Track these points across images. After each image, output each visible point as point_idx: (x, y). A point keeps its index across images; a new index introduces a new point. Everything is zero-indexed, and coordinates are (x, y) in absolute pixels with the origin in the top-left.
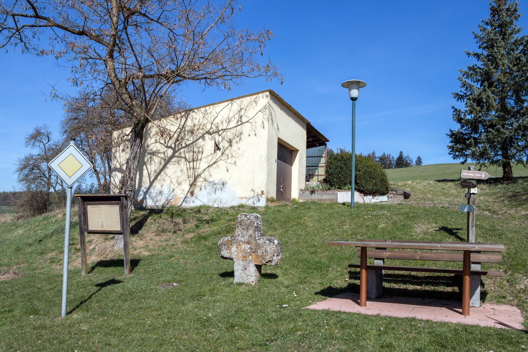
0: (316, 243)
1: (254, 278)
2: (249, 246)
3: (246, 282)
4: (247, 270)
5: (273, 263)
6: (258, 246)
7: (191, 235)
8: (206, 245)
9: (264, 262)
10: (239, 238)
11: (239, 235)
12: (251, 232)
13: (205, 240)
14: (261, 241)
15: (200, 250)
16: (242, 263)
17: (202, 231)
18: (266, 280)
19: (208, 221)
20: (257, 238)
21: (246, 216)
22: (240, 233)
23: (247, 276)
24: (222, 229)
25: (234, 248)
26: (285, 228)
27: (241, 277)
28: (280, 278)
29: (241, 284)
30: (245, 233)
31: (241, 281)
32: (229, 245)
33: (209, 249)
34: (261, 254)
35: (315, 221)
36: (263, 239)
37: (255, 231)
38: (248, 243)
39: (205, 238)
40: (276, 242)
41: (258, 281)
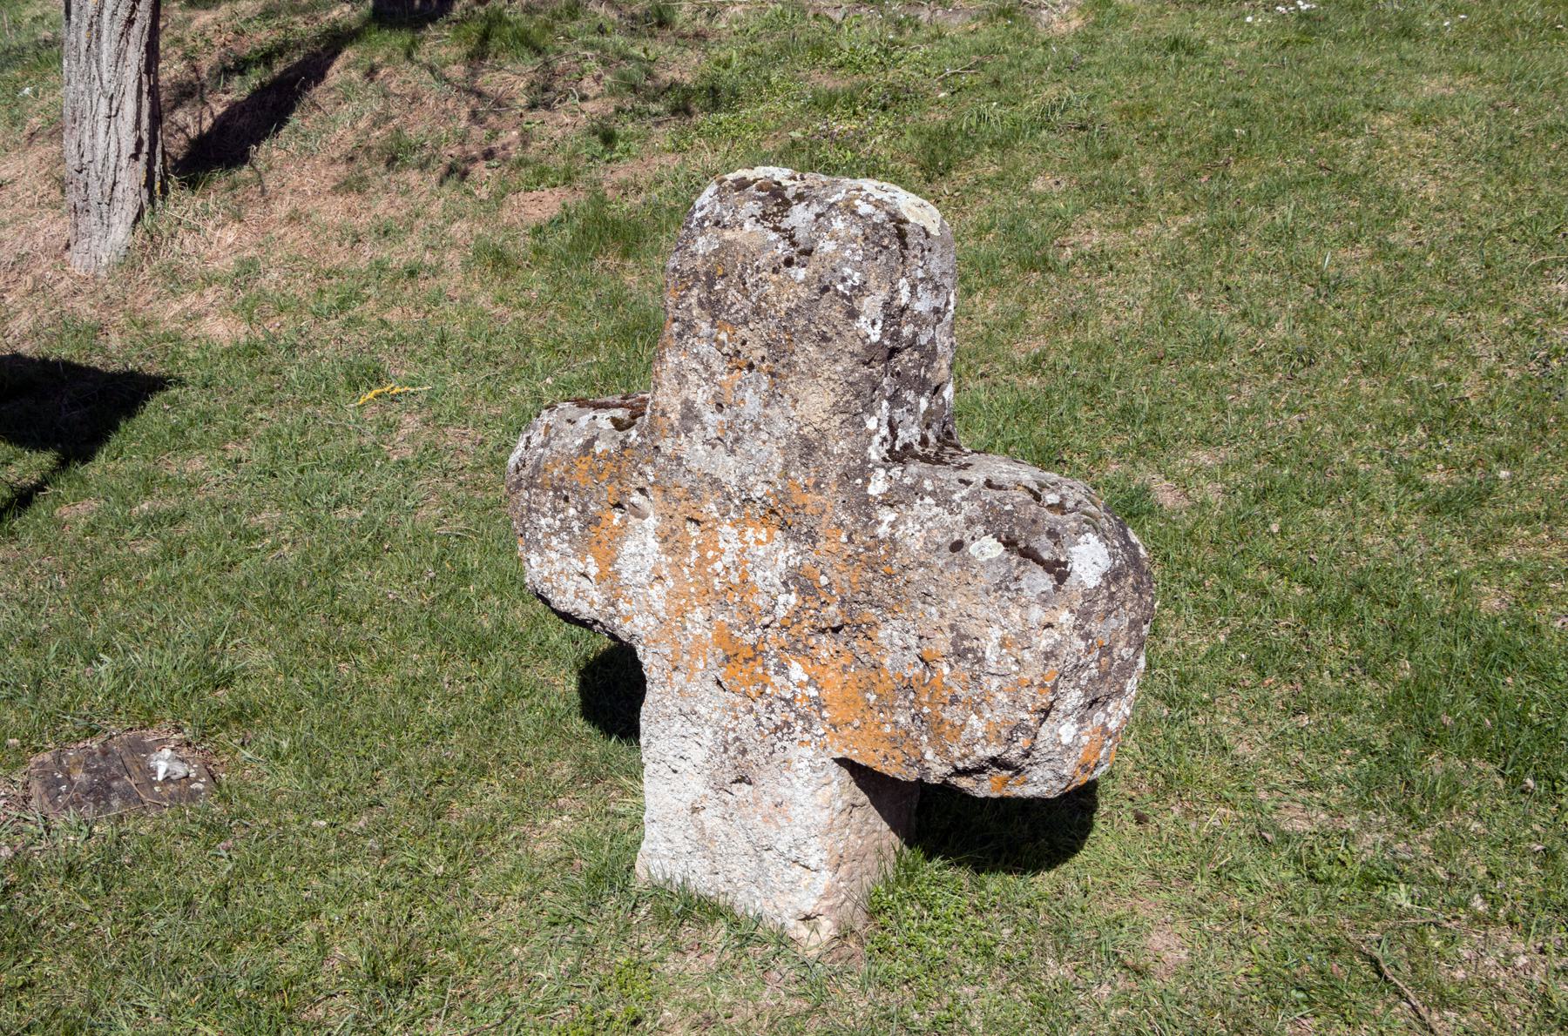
0: (1470, 387)
1: (825, 879)
3: (748, 901)
6: (882, 575)
7: (545, 204)
10: (696, 453)
12: (815, 403)
14: (914, 529)
16: (711, 703)
18: (950, 885)
19: (688, 94)
20: (877, 487)
22: (701, 397)
23: (760, 849)
25: (641, 548)
27: (704, 842)
30: (752, 403)
31: (702, 881)
32: (593, 498)
35: (1464, 155)
36: (943, 499)
37: (860, 398)
38: (781, 515)
40: (1090, 559)
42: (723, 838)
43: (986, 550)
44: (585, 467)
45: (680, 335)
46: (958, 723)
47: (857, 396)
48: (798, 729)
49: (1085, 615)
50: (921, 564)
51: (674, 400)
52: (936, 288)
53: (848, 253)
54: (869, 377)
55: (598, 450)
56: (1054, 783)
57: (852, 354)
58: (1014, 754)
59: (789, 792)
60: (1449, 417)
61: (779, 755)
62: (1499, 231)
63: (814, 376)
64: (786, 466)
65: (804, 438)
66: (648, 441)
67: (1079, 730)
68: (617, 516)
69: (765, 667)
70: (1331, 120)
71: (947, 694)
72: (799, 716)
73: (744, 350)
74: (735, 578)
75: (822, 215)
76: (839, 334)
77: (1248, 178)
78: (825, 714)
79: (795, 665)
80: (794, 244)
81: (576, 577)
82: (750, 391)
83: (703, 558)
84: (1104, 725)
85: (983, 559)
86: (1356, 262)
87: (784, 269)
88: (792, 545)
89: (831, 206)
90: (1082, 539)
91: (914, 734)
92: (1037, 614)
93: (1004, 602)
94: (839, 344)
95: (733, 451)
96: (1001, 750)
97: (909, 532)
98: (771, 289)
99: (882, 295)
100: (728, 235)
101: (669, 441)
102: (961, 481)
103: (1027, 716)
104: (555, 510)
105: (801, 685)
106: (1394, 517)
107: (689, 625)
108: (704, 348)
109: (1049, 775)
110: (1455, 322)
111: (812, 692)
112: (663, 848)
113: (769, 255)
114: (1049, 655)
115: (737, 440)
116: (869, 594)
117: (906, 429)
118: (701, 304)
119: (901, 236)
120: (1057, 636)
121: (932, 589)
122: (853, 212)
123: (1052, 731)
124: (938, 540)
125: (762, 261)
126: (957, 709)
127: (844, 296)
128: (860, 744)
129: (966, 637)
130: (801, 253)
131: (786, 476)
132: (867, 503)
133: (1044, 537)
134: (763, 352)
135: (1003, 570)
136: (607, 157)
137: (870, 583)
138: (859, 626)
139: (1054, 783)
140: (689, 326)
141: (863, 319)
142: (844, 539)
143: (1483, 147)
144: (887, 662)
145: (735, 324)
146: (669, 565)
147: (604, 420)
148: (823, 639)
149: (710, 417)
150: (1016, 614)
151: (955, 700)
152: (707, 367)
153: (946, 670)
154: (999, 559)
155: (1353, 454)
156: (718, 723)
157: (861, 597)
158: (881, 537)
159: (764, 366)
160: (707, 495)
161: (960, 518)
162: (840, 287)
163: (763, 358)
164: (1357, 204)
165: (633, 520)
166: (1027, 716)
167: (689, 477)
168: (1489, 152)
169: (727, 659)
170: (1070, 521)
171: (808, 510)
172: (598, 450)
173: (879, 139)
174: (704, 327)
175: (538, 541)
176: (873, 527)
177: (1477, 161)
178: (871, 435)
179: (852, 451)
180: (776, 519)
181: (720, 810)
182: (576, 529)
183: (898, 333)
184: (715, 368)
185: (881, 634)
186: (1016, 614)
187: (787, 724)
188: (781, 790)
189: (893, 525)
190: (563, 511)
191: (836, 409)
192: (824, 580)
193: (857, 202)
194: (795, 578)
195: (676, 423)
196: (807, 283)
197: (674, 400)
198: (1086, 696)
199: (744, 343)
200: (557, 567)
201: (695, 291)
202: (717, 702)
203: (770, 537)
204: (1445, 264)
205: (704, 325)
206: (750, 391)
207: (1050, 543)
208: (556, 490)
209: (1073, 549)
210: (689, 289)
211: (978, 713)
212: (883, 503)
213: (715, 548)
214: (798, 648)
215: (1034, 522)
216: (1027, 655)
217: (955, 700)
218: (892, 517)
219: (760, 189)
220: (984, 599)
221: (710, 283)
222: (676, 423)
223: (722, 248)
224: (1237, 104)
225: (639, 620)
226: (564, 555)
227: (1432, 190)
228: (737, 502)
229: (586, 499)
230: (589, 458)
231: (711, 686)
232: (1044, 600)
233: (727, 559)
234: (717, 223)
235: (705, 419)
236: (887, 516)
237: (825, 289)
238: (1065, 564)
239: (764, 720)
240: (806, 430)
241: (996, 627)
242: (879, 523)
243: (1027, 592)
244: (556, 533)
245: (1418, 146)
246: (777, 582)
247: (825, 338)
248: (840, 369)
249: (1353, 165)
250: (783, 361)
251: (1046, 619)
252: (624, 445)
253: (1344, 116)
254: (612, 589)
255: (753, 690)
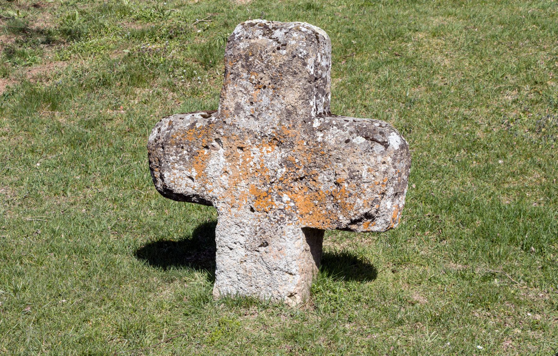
1: (298, 278)
2: (279, 154)
3: (264, 294)
4: (273, 248)
5: (379, 226)
8: (58, 130)
9: (345, 222)
10: (242, 121)
11: (239, 107)
12: (291, 97)
13: (54, 107)
14: (332, 137)
15: (38, 142)
16: (248, 218)
17: (36, 71)
20: (316, 124)
21: (268, 31)
22: (243, 100)
24: (111, 66)
25: (217, 160)
26: (351, 71)
27: (246, 276)
28: (385, 275)
29: (244, 303)
30: (265, 100)
31: (246, 290)
33: (72, 143)
34: (333, 188)
36: (340, 126)
38: (277, 141)
39: (53, 101)
41: (313, 292)
42: (255, 270)
43: (359, 140)
44: (192, 133)
45: (234, 79)
46: (352, 203)
47: (307, 94)
48: (287, 219)
49: (394, 159)
50: (335, 149)
51: (232, 103)
52: (327, 58)
53: (301, 44)
54: (310, 87)
55: (198, 127)
56: (384, 225)
57: (305, 78)
58: (373, 212)
59: (284, 244)
60: (474, 145)
61: (280, 231)
62: (479, 77)
63: (292, 87)
64: (280, 121)
65: (287, 110)
66: (221, 120)
67: (392, 204)
68: (206, 151)
69: (272, 198)
70: (397, 35)
71: (347, 194)
72: (287, 215)
73: (262, 81)
74: (259, 167)
75: (287, 33)
76: (300, 71)
77: (363, 61)
78: (298, 211)
79: (285, 195)
80: (279, 43)
81: (186, 179)
82: (265, 96)
83: (245, 161)
84: (398, 205)
85: (359, 143)
86: (420, 92)
87: (277, 51)
88: (283, 150)
89: (290, 29)
90: (391, 134)
91: (335, 211)
92: (380, 159)
93: (368, 156)
94: (300, 75)
95: (258, 119)
96: (369, 209)
97: (330, 138)
98: (273, 58)
99: (314, 58)
100: (252, 41)
101: (230, 119)
102: (345, 121)
103: (377, 196)
104: (177, 153)
105: (288, 202)
106: (461, 180)
107: (239, 188)
108: (244, 82)
109: (383, 221)
110: (467, 113)
111: (292, 204)
112: (227, 281)
113: (270, 47)
114: (385, 172)
115: (259, 114)
116: (315, 163)
117: (320, 107)
118: (243, 66)
119: (317, 38)
120: (387, 166)
121: (340, 156)
122: (300, 31)
123: (384, 203)
124: (341, 140)
125: (268, 49)
126: (352, 198)
127: (301, 58)
128: (313, 220)
129: (354, 171)
130: (282, 45)
131: (281, 125)
132: (313, 130)
133: (378, 134)
134: (269, 81)
135: (366, 146)
136: (24, 63)
137: (315, 159)
138: (311, 176)
139: (384, 225)
140: (238, 75)
141: (308, 66)
142: (305, 144)
143: (466, 45)
144: (322, 188)
145: (257, 72)
146: (230, 166)
147: (198, 116)
148: (296, 183)
149: (247, 107)
150: (373, 160)
151: (351, 195)
152: (246, 89)
153: (346, 185)
154: (364, 142)
155: (438, 160)
156: (252, 225)
157: (312, 165)
158: (319, 141)
159: (270, 86)
160: (246, 137)
161: (347, 132)
162: (300, 55)
163: (270, 84)
164: (415, 70)
165: (213, 152)
166: (377, 196)
167: (239, 131)
168: (468, 47)
169: (256, 198)
170: (387, 129)
171: (290, 136)
172: (198, 127)
173: (174, 52)
174: (245, 75)
175: (168, 167)
176: (316, 138)
177: (464, 50)
178: (311, 107)
179: (306, 113)
180: (275, 142)
181: (254, 259)
182: (187, 159)
183: (317, 72)
184: (249, 89)
185: (319, 178)
186: (373, 160)
187: (282, 218)
188: (281, 244)
189: (323, 137)
190: (181, 152)
191: (301, 98)
192: (297, 161)
193: (301, 27)
194: (285, 162)
195: (233, 112)
196: (287, 55)
197: (232, 103)
198: (394, 191)
199: (261, 79)
200: (178, 175)
201: (240, 62)
202: (250, 217)
203: (273, 149)
204: (459, 91)
205: (244, 74)
206: (265, 96)
207: (381, 136)
208: (177, 145)
209: (389, 137)
210: (237, 61)
211: (360, 198)
212: (318, 130)
213: (250, 157)
214: (288, 189)
215: (374, 130)
216: (377, 174)
217: (351, 195)
218: (322, 135)
219: (260, 25)
220: (361, 156)
221: (247, 58)
222: (233, 112)
223: (251, 46)
224: (349, 31)
225: (216, 191)
226: (181, 170)
227: (447, 62)
228: (259, 138)
229: (192, 146)
230: (194, 130)
231: (248, 211)
232: (382, 154)
233: (255, 160)
234: (247, 38)
235: (245, 109)
236: (320, 135)
237: (294, 56)
238: (387, 142)
239: (272, 219)
240: (288, 107)
241: (365, 165)
242: (318, 137)
243: (376, 152)
244: (177, 162)
245: (437, 45)
246: (277, 165)
247: (296, 73)
248: (301, 84)
249: (410, 53)
250: (278, 83)
251: (383, 160)
252: (210, 123)
253: (402, 34)
254: (203, 180)
255: (267, 208)
